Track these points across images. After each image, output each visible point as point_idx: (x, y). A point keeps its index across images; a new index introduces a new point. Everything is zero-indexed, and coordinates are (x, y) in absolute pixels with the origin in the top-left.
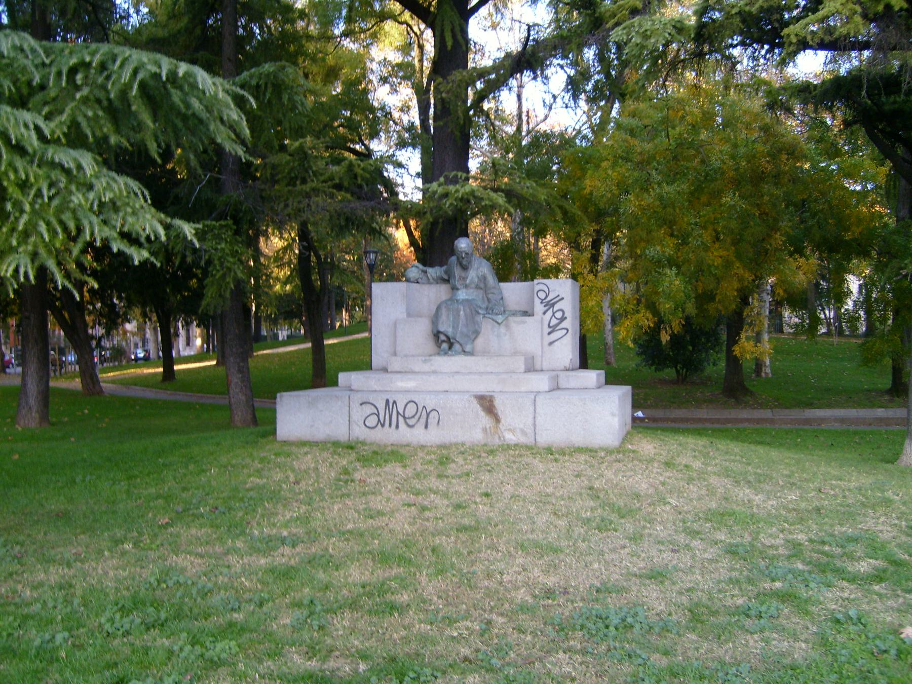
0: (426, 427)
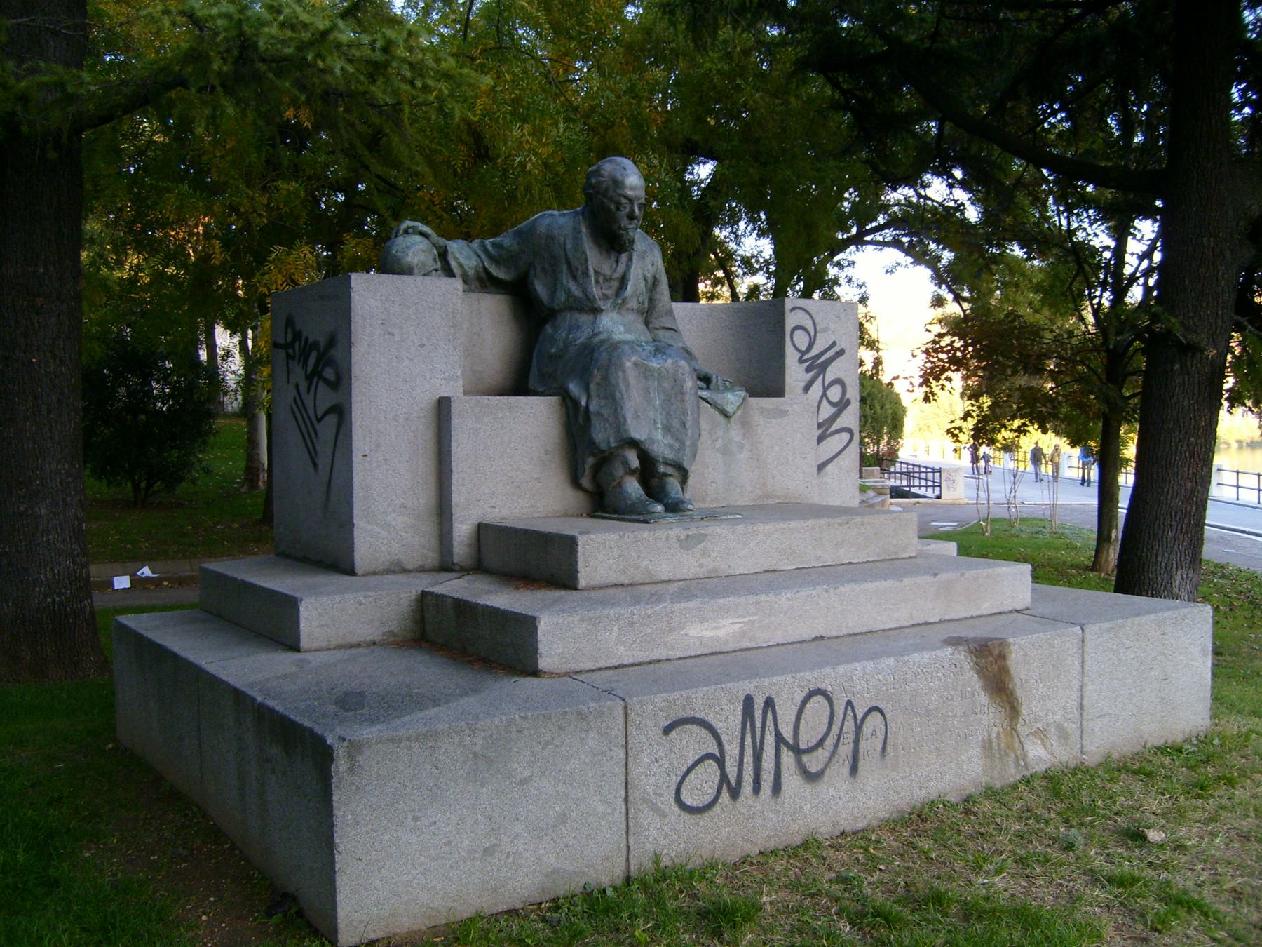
0: (854, 770)
